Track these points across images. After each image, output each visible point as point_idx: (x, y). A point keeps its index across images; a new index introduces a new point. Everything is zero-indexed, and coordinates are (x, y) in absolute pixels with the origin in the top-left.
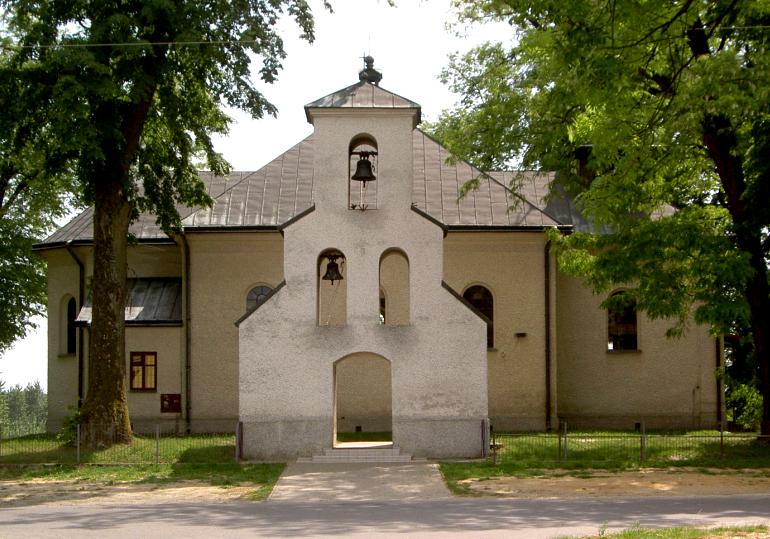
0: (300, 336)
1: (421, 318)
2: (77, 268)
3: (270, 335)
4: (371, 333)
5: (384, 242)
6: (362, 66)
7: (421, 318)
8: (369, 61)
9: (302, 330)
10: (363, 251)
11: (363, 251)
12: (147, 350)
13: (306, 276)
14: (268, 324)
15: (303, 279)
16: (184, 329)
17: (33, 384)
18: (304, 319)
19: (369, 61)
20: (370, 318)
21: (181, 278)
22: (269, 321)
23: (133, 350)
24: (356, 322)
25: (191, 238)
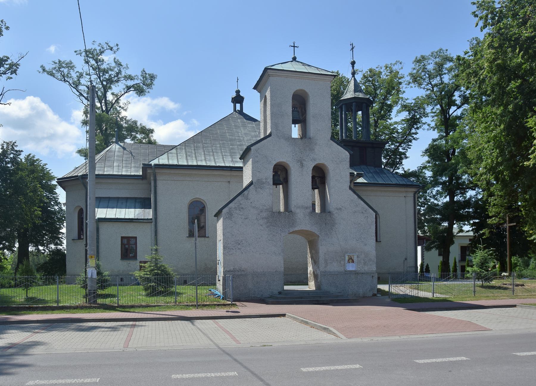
0: (263, 218)
1: (337, 209)
2: (84, 192)
3: (243, 217)
4: (307, 218)
5: (315, 160)
6: (234, 95)
7: (337, 209)
8: (238, 92)
9: (264, 214)
10: (302, 165)
11: (302, 165)
12: (130, 236)
13: (266, 179)
14: (242, 210)
15: (264, 181)
16: (153, 224)
17: (155, 74)
18: (265, 208)
19: (238, 92)
20: (307, 208)
21: (150, 199)
22: (242, 208)
23: (124, 235)
24: (298, 211)
25: (157, 171)
